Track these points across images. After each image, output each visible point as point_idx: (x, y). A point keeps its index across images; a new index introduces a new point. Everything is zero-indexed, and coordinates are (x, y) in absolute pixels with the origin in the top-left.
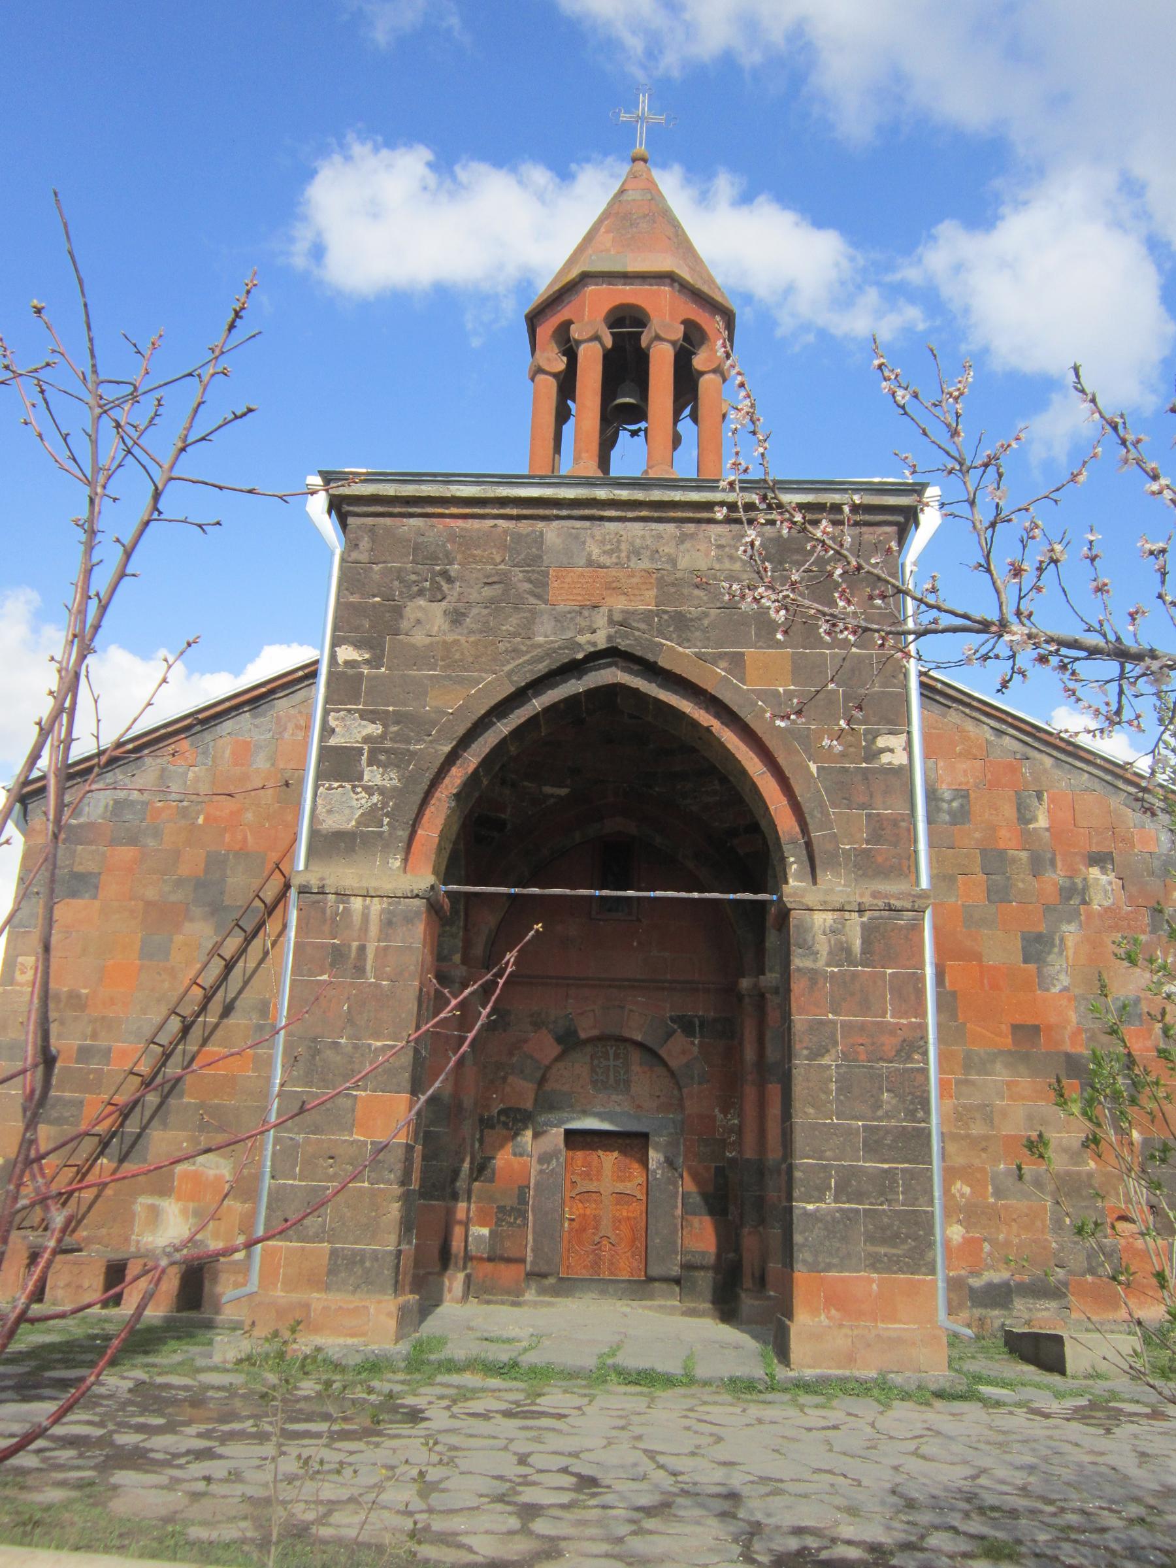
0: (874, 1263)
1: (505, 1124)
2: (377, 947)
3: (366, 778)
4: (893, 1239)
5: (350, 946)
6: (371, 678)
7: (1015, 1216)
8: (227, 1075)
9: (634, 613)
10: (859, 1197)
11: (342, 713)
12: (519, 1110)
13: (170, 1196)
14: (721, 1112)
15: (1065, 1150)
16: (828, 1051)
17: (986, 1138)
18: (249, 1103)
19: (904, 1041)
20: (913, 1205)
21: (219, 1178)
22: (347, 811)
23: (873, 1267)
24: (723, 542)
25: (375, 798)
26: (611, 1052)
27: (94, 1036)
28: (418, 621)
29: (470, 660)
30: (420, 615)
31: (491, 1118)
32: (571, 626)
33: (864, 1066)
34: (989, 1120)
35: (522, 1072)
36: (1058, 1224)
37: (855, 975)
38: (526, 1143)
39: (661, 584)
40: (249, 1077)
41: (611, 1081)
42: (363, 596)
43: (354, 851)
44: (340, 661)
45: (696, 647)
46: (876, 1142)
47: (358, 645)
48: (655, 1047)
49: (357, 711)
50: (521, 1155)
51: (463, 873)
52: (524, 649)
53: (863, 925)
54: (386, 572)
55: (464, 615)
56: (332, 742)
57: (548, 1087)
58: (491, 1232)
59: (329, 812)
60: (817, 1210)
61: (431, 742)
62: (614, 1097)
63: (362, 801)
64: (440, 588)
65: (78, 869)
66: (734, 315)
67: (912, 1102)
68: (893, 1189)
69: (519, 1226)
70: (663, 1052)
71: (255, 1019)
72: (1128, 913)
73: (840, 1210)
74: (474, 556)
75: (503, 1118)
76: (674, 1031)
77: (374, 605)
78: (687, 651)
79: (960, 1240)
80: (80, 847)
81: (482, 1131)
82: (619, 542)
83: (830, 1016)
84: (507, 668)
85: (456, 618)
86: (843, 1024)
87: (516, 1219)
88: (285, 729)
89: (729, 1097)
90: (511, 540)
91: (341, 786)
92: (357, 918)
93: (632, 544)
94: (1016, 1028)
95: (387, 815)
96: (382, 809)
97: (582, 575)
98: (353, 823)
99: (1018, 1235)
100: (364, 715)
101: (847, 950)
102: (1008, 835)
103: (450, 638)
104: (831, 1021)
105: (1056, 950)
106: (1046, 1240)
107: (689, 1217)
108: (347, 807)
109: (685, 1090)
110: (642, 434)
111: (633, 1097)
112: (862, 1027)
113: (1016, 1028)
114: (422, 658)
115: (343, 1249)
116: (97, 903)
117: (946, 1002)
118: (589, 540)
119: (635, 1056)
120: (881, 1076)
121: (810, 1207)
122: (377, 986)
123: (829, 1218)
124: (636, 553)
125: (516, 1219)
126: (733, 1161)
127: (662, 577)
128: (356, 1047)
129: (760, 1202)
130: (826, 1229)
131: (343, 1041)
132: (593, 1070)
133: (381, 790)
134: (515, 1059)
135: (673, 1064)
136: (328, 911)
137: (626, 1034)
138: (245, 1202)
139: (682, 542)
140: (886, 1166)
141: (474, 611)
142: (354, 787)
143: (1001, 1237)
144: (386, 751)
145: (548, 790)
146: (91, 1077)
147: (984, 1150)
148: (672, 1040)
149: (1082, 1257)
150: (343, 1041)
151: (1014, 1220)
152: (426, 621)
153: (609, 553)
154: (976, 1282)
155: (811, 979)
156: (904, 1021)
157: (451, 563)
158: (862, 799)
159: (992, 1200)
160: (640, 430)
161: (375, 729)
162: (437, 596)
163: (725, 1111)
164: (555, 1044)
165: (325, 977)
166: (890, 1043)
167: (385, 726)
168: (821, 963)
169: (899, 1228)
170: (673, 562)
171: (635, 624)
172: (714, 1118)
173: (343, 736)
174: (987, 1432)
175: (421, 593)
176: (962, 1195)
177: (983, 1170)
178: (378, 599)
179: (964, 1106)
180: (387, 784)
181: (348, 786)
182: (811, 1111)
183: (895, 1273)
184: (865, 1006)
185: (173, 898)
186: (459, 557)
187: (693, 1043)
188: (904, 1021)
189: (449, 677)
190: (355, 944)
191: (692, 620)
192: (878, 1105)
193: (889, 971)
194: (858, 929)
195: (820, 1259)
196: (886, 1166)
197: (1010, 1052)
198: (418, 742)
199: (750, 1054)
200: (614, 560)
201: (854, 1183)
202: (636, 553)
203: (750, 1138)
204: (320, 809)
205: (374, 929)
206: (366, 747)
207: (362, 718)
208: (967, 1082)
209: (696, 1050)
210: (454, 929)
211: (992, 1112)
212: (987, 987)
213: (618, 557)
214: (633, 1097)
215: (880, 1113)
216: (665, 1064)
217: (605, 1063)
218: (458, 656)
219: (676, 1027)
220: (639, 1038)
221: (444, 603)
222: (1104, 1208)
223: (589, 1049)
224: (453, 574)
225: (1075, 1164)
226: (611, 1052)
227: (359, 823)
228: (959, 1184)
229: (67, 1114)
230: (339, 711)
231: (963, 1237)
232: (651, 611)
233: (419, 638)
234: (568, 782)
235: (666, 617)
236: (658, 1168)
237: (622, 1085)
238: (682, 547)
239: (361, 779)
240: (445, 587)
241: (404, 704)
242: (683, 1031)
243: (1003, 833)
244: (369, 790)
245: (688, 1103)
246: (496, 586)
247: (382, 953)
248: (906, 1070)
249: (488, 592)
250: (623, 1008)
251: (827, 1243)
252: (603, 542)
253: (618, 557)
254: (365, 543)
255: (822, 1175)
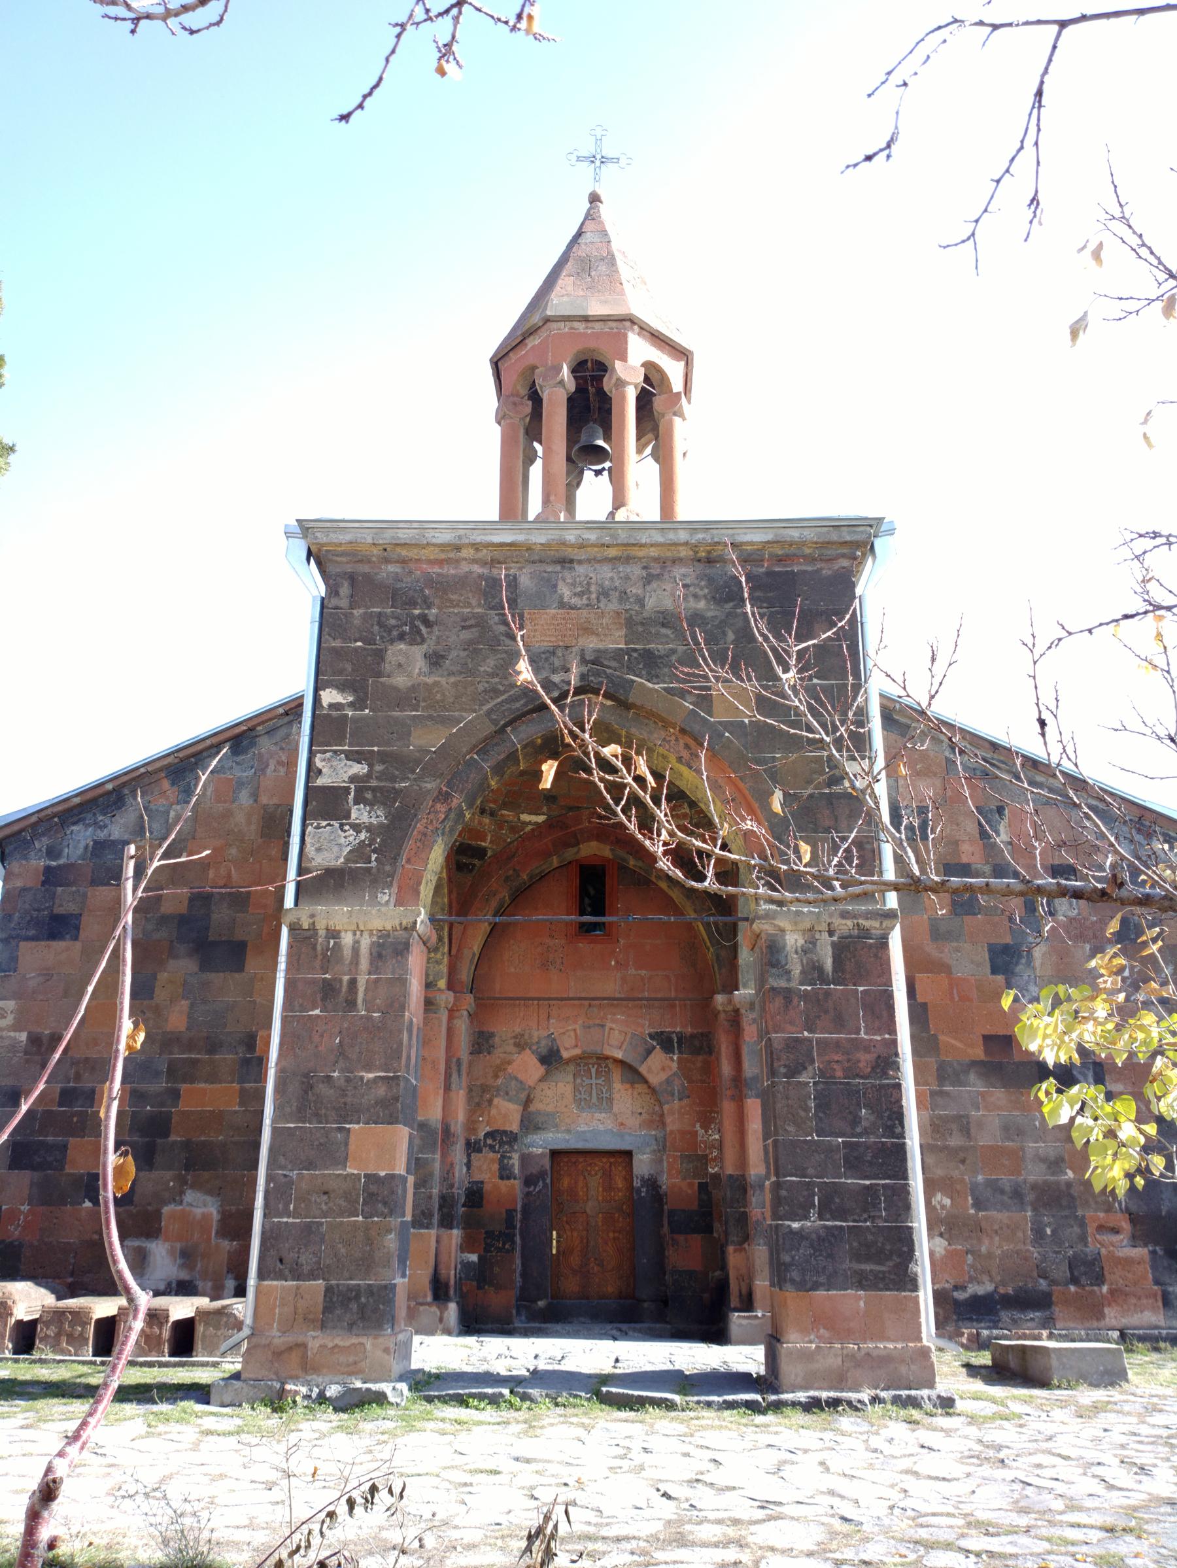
0: (862, 1281)
1: (492, 1147)
2: (368, 980)
3: (353, 816)
4: (878, 1256)
5: (341, 981)
6: (355, 720)
7: (996, 1227)
8: (214, 1111)
9: (605, 651)
10: (841, 1214)
11: (328, 755)
12: (505, 1132)
13: (157, 1238)
14: (701, 1127)
15: (1043, 1160)
16: (805, 1068)
17: (962, 1149)
18: (236, 1138)
19: (879, 1057)
20: (896, 1221)
21: (206, 1217)
22: (335, 849)
23: (860, 1286)
24: (688, 581)
25: (363, 836)
26: (593, 1071)
27: (78, 1077)
28: (400, 665)
29: (451, 700)
30: (402, 660)
31: (477, 1142)
32: (546, 665)
33: (841, 1083)
34: (966, 1130)
35: (507, 1094)
36: (1039, 1233)
37: (828, 993)
38: (513, 1165)
39: (630, 623)
40: (236, 1112)
41: (594, 1100)
42: (344, 640)
43: (343, 886)
44: (325, 704)
45: (665, 682)
46: (856, 1158)
47: (342, 688)
48: (635, 1064)
49: (342, 752)
50: (508, 1178)
51: (446, 900)
52: (502, 688)
53: (833, 944)
54: (367, 617)
55: (443, 657)
56: (320, 782)
57: (532, 1108)
58: (480, 1258)
59: (318, 850)
60: (802, 1228)
61: (415, 779)
62: (597, 1115)
63: (348, 839)
64: (419, 632)
65: (58, 910)
66: (691, 353)
67: (890, 1118)
68: (876, 1206)
69: (508, 1251)
70: (643, 1069)
71: (242, 1052)
72: (1093, 923)
73: (825, 1227)
74: (451, 601)
75: (489, 1141)
76: (654, 1048)
77: (356, 649)
78: (656, 686)
79: (943, 1252)
80: (59, 889)
81: (469, 1156)
82: (589, 584)
83: (806, 1033)
84: (485, 708)
85: (435, 660)
86: (819, 1041)
87: (504, 1244)
88: (267, 766)
89: (708, 1115)
90: (487, 585)
91: (329, 825)
92: (347, 953)
93: (601, 586)
94: (987, 1039)
95: (374, 851)
96: (370, 845)
97: (554, 617)
98: (342, 860)
99: (1000, 1247)
100: (350, 756)
101: (820, 969)
102: (971, 849)
103: (430, 680)
104: (806, 1039)
105: (1023, 961)
106: (1028, 1250)
107: (676, 1236)
108: (332, 845)
109: (666, 1107)
110: (606, 473)
111: (616, 1115)
112: (837, 1044)
113: (987, 1039)
114: (405, 699)
115: (338, 1285)
116: (78, 945)
117: (918, 1013)
118: (560, 583)
119: (616, 1074)
120: (858, 1092)
121: (795, 1225)
122: (368, 1018)
123: (814, 1236)
124: (604, 593)
125: (504, 1244)
126: (716, 1177)
127: (631, 617)
128: (348, 1080)
129: (743, 1219)
130: (812, 1246)
131: (336, 1074)
132: (576, 1089)
133: (369, 828)
134: (499, 1081)
135: (655, 1079)
136: (319, 948)
137: (608, 1051)
138: (232, 1240)
139: (649, 583)
140: (867, 1182)
141: (454, 654)
142: (341, 826)
143: (984, 1249)
144: (374, 790)
145: (525, 817)
146: (75, 1119)
147: (963, 1161)
148: (653, 1055)
149: (1065, 1267)
150: (336, 1074)
151: (996, 1232)
152: (407, 664)
153: (580, 595)
154: (960, 1296)
155: (785, 998)
156: (878, 1038)
157: (429, 608)
158: (827, 823)
159: (972, 1211)
160: (604, 469)
161: (360, 769)
162: (415, 638)
163: (706, 1128)
164: (538, 1064)
165: (317, 1012)
166: (865, 1060)
167: (371, 766)
168: (794, 985)
169: (883, 1244)
170: (640, 601)
171: (606, 663)
172: (695, 1134)
173: (330, 776)
174: (978, 1448)
175: (401, 637)
176: (943, 1207)
177: (963, 1181)
178: (359, 644)
179: (940, 1117)
180: (374, 821)
181: (336, 824)
182: (791, 1129)
183: (881, 1290)
184: (839, 1023)
185: (157, 936)
186: (437, 601)
187: (672, 1059)
188: (878, 1038)
189: (430, 717)
190: (346, 978)
191: (660, 657)
192: (856, 1120)
193: (861, 989)
194: (829, 948)
195: (807, 1278)
196: (867, 1182)
197: (982, 1063)
198: (404, 779)
199: (726, 1069)
200: (585, 601)
201: (837, 1200)
202: (604, 593)
203: (730, 1155)
204: (310, 849)
205: (364, 964)
206: (352, 786)
207: (348, 758)
208: (941, 1093)
209: (675, 1065)
210: (439, 956)
211: (968, 1123)
212: (957, 998)
213: (589, 599)
214: (616, 1115)
215: (858, 1130)
216: (646, 1082)
217: (587, 1081)
218: (438, 697)
219: (655, 1043)
220: (619, 1055)
221: (425, 646)
222: (1084, 1217)
223: (572, 1068)
224: (431, 618)
225: (1053, 1174)
226: (593, 1071)
227: (347, 860)
228: (939, 1196)
229: (50, 1159)
230: (325, 752)
231: (945, 1249)
232: (621, 649)
233: (400, 681)
234: (545, 809)
235: (635, 655)
236: (642, 1186)
237: (605, 1102)
238: (648, 588)
239: (348, 816)
240: (424, 630)
241: (388, 744)
242: (662, 1048)
243: (966, 847)
244: (357, 828)
245: (668, 1120)
246: (474, 630)
247: (372, 986)
248: (882, 1086)
249: (466, 635)
250: (603, 1026)
251: (814, 1262)
252: (574, 585)
253: (589, 599)
254: (345, 590)
255: (805, 1193)
